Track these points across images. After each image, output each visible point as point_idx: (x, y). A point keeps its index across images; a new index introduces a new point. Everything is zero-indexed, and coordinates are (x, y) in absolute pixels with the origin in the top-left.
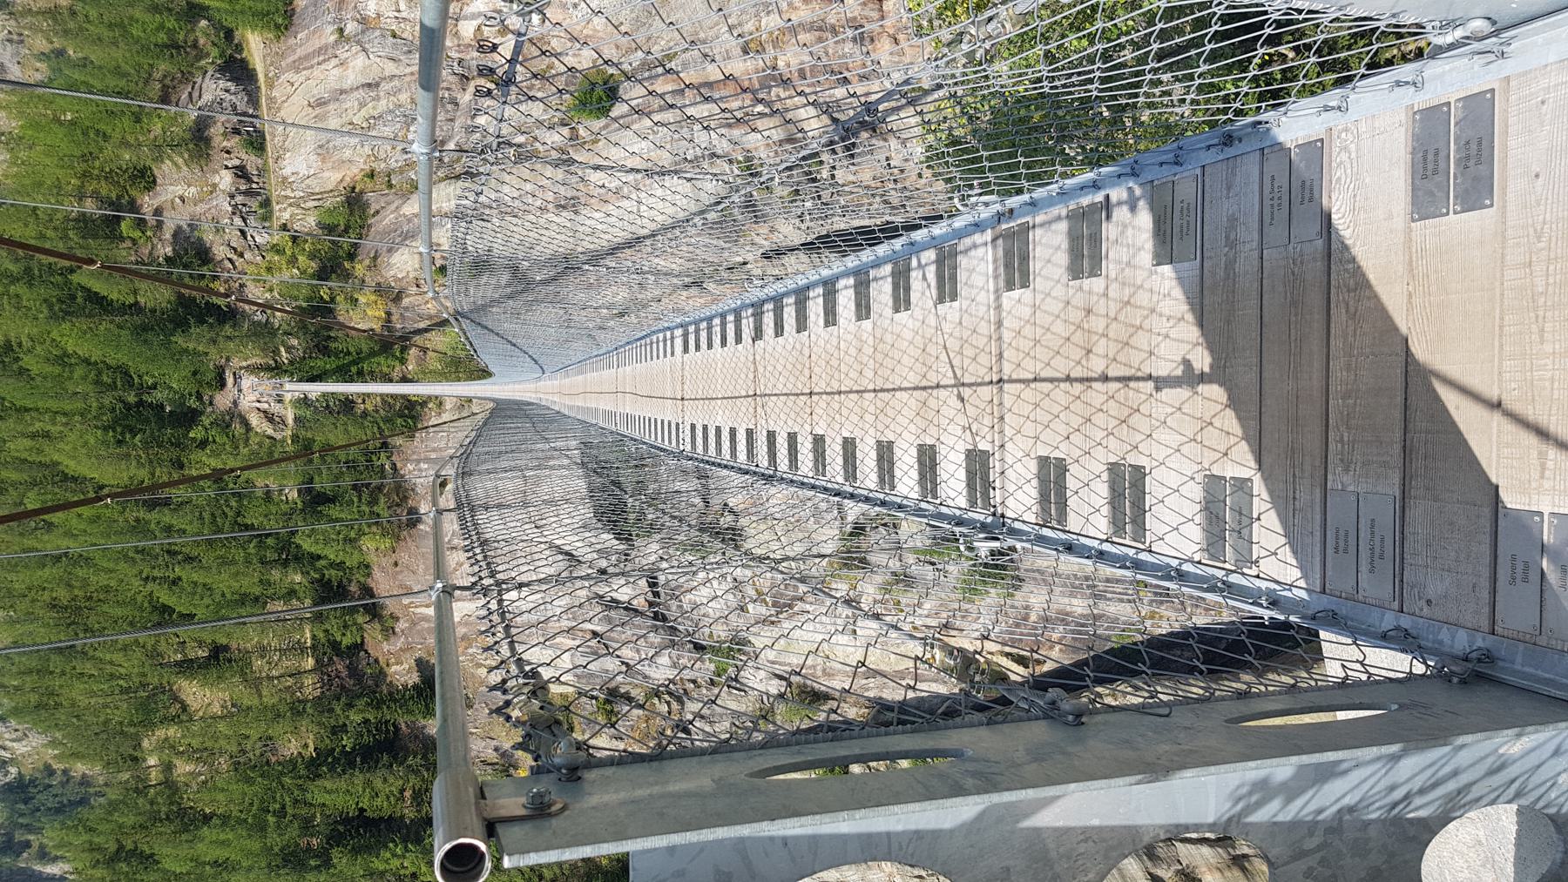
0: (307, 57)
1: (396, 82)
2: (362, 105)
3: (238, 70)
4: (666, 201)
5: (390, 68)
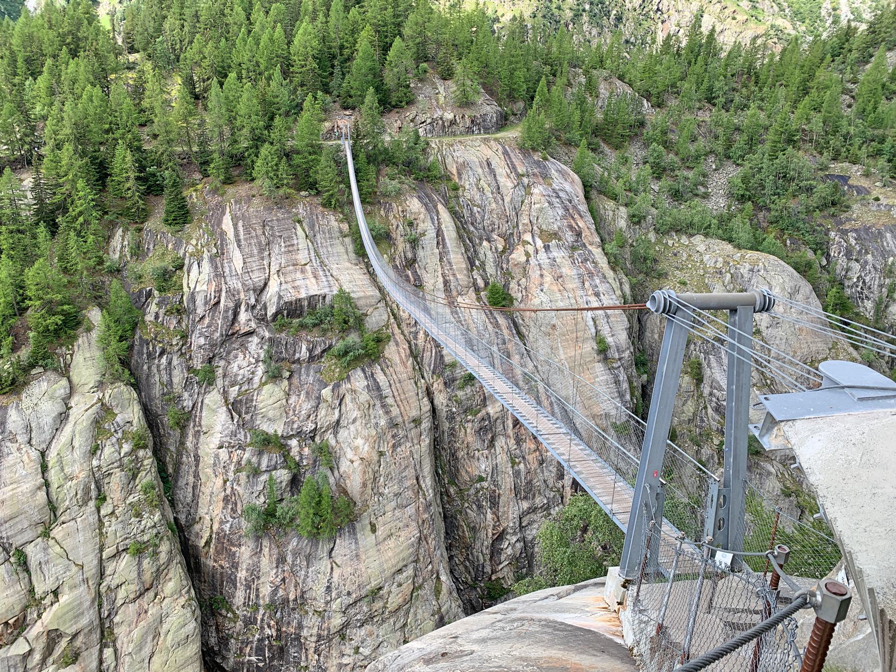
0: (510, 158)
1: (501, 202)
3: (503, 122)
5: (507, 199)
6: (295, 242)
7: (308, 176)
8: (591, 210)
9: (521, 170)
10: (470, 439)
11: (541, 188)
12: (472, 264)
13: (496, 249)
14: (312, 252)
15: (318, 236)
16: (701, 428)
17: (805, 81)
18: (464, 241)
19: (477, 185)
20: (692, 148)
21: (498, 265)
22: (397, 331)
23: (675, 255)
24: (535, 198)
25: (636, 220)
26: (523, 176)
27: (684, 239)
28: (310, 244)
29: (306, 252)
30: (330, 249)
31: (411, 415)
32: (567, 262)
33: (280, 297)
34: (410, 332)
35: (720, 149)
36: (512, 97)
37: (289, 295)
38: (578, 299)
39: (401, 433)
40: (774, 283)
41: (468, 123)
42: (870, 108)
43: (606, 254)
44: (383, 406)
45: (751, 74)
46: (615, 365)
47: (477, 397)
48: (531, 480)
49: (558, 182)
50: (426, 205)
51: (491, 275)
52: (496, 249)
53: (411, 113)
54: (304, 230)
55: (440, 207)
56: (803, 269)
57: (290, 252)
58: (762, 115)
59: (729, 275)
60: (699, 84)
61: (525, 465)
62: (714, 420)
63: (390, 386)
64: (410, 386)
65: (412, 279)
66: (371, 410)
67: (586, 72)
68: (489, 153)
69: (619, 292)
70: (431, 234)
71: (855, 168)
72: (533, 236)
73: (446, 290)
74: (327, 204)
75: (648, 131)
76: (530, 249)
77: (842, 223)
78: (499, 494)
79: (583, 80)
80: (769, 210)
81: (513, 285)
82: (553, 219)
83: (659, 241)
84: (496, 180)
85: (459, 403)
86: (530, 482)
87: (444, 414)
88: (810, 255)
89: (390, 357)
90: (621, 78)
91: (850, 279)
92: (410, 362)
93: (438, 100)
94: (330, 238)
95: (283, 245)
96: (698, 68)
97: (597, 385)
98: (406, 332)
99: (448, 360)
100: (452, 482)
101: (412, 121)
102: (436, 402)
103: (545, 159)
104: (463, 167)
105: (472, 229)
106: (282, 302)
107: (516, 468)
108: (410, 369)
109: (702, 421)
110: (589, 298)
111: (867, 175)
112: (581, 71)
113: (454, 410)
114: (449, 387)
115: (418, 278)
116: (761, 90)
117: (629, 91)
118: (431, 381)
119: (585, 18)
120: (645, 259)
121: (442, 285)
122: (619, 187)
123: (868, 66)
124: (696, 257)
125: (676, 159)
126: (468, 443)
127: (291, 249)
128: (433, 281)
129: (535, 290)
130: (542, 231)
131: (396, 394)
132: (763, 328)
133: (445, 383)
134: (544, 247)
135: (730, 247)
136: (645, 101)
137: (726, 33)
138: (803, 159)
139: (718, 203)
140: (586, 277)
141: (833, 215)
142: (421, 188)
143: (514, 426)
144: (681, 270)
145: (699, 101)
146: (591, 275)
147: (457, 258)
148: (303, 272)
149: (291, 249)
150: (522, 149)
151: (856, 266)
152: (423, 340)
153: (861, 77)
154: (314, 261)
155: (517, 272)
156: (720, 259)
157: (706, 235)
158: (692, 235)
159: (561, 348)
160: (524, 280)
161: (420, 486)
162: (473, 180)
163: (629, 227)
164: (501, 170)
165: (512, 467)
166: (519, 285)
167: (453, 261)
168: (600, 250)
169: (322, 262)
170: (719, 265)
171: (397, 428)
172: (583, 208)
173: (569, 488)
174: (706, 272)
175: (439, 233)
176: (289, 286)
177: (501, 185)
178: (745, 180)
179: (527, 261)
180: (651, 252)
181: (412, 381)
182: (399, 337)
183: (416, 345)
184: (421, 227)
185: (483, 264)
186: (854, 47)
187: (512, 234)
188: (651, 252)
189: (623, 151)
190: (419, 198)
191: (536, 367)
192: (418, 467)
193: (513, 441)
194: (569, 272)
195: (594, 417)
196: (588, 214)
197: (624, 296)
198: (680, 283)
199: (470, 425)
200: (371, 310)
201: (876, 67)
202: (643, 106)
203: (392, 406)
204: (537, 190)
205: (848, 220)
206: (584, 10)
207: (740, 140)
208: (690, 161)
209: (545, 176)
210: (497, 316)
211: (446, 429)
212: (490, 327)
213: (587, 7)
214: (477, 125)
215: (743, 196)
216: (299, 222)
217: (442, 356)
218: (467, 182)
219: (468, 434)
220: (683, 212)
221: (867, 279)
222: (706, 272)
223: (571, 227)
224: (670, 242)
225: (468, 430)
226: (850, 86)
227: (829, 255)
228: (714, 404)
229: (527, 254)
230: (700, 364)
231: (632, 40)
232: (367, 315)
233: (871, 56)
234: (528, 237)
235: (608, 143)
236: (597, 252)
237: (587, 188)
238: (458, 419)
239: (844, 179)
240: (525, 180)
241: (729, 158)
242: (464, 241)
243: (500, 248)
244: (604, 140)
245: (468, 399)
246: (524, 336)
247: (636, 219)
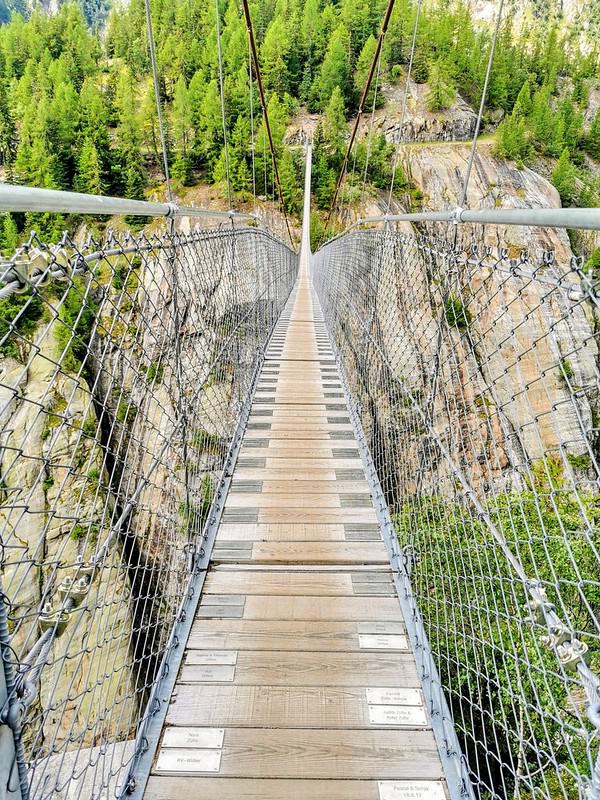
0: (481, 167)
3: (482, 128)
11: (512, 199)
93: (407, 103)
99: (394, 375)
101: (379, 126)
103: (520, 169)
104: (429, 175)
142: (382, 196)
150: (496, 157)
162: (439, 189)
177: (468, 195)
199: (413, 444)
209: (519, 187)
214: (449, 131)
223: (542, 243)
244: (589, 154)
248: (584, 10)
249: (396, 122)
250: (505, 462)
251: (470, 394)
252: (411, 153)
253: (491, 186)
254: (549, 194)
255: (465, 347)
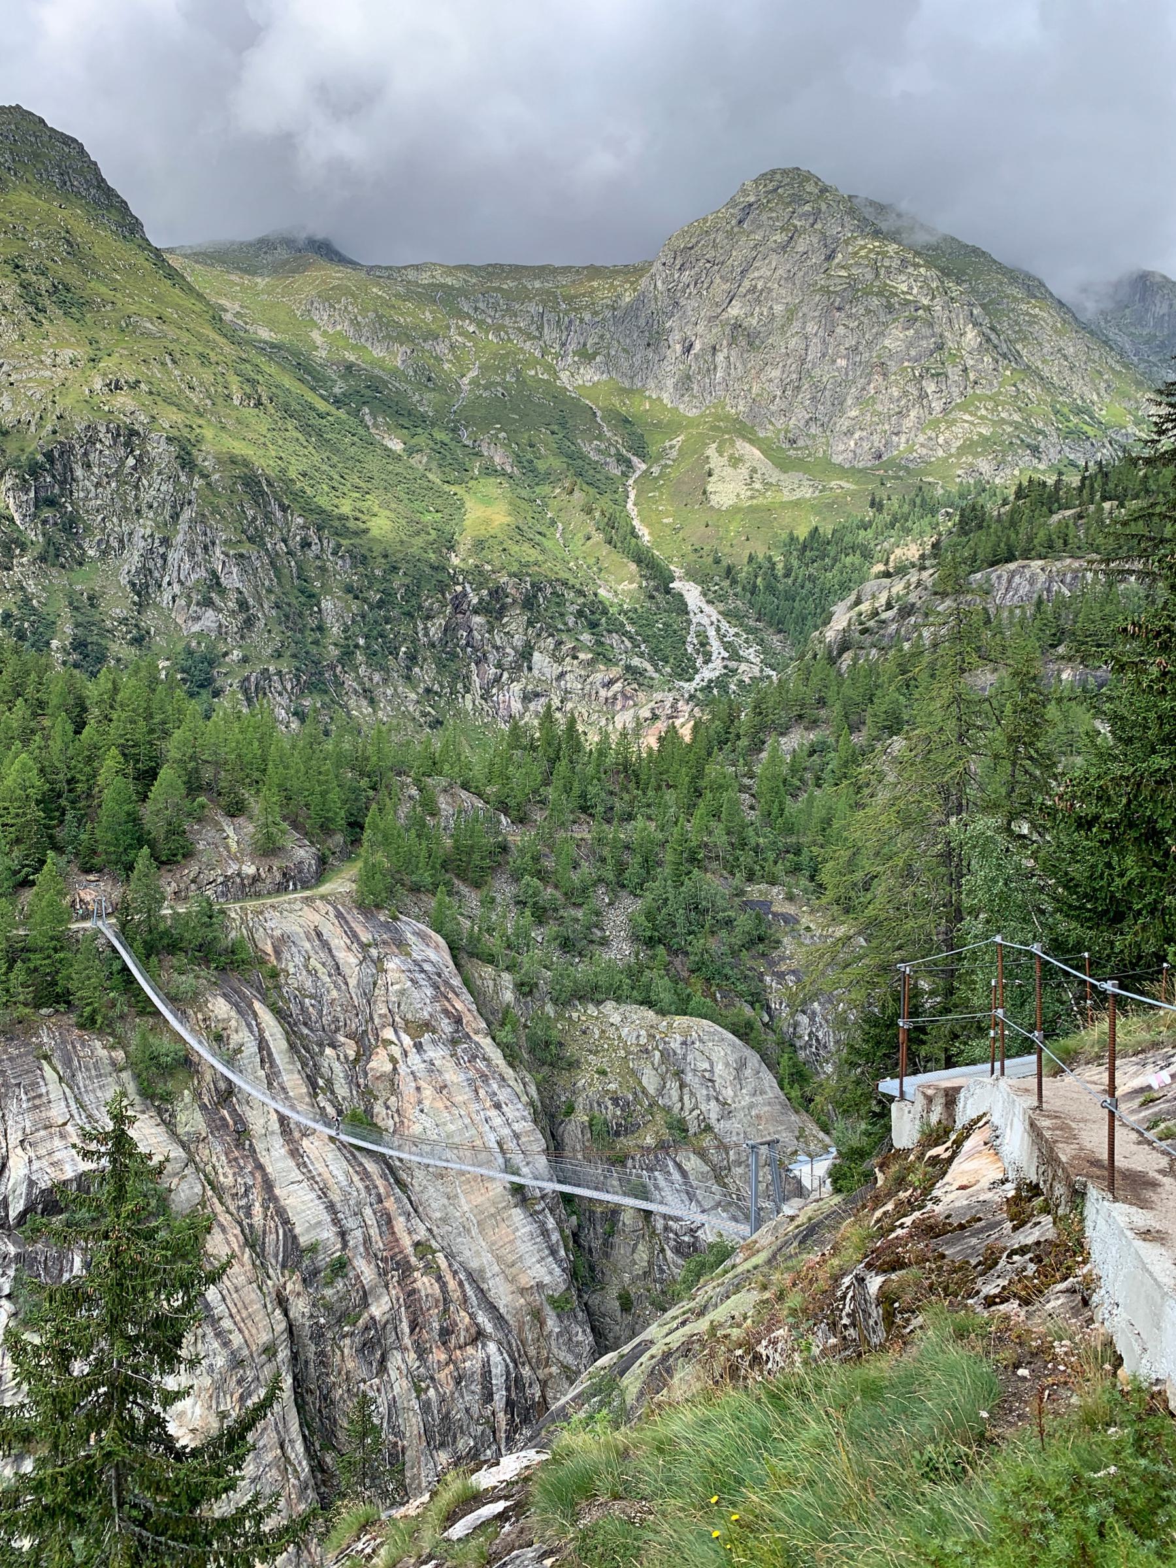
0: (347, 922)
1: (344, 987)
2: (324, 964)
3: (323, 868)
4: (304, 1208)
5: (353, 982)
6: (43, 1090)
7: (54, 983)
8: (466, 982)
9: (365, 937)
10: (350, 1365)
11: (397, 960)
12: (313, 1085)
13: (346, 1057)
14: (72, 1102)
15: (79, 1076)
16: (662, 1281)
17: (694, 778)
18: (297, 1052)
19: (306, 967)
20: (575, 877)
21: (352, 1081)
22: (219, 1208)
23: (584, 1033)
24: (391, 976)
25: (525, 988)
26: (369, 946)
27: (592, 1010)
28: (67, 1090)
29: (63, 1103)
30: (99, 1094)
31: (260, 1342)
32: (450, 1064)
33: (32, 1184)
34: (239, 1208)
35: (611, 877)
36: (326, 829)
37: (46, 1177)
38: (474, 1116)
39: (250, 1374)
40: (714, 1059)
41: (278, 877)
42: (775, 811)
43: (498, 1045)
44: (218, 1335)
45: (628, 771)
46: (538, 1208)
47: (354, 1294)
48: (448, 1413)
49: (419, 950)
50: (236, 1005)
51: (344, 1099)
52: (346, 1057)
53: (192, 870)
54: (55, 1069)
55: (257, 1005)
56: (743, 1031)
57: (36, 1107)
58: (652, 826)
59: (657, 1053)
60: (568, 790)
61: (436, 1389)
62: (677, 1267)
63: (224, 1299)
64: (251, 1294)
65: (231, 1122)
66: (199, 1345)
67: (417, 782)
68: (316, 918)
69: (525, 1099)
70: (251, 1048)
71: (775, 890)
72: (396, 1032)
73: (283, 1133)
74: (88, 1023)
75: (514, 860)
76: (396, 1051)
77: (775, 964)
78: (403, 1447)
79: (414, 791)
80: (686, 954)
81: (378, 1108)
82: (422, 1002)
83: (560, 1016)
84: (333, 956)
85: (329, 1308)
86: (446, 1417)
87: (307, 1332)
88: (748, 1011)
89: (215, 1252)
90: (465, 786)
91: (800, 1037)
92: (247, 1256)
93: (228, 847)
94: (97, 1077)
95: (24, 1097)
96: (562, 767)
97: (518, 1242)
98: (232, 1209)
99: (304, 1241)
100: (328, 1446)
101: (193, 881)
102: (291, 1315)
103: (396, 919)
104: (282, 943)
105: (306, 1031)
106: (36, 1191)
107: (424, 1397)
108: (249, 1267)
109: (662, 1271)
110: (489, 1113)
111: (790, 898)
112: (409, 780)
113: (322, 1321)
114: (311, 1286)
115: (239, 1119)
116: (644, 793)
117: (480, 804)
118: (282, 1280)
119: (360, 657)
120: (547, 1044)
121: (277, 1125)
122: (493, 943)
123: (764, 755)
124: (611, 1032)
125: (558, 894)
126: (348, 1372)
127: (37, 1102)
128: (262, 1121)
129: (411, 1112)
130: (407, 1022)
131: (234, 1311)
132: (713, 1122)
133: (304, 1280)
134: (415, 1045)
135: (651, 1013)
136: (502, 817)
137: (567, 677)
138: (713, 884)
139: (620, 951)
140: (479, 1083)
141: (763, 955)
142: (224, 981)
143: (412, 1331)
144: (596, 1053)
145: (572, 812)
146: (485, 1078)
147: (293, 1080)
148: (63, 1136)
149: (37, 1102)
150: (361, 907)
151: (804, 1020)
152: (261, 1216)
153: (758, 769)
154: (77, 1117)
155: (381, 1088)
156: (643, 1032)
157: (618, 1000)
158: (599, 1003)
159: (461, 1195)
160: (393, 1099)
161: (288, 1460)
162: (299, 960)
163: (517, 1000)
164: (338, 941)
165: (418, 1397)
166: (388, 1108)
167: (287, 1085)
168: (489, 1040)
169: (89, 1116)
170: (643, 1041)
171: (243, 1367)
172: (456, 982)
173: (502, 1414)
174: (628, 1053)
175: (263, 1045)
176: (44, 1163)
177: (341, 962)
178: (650, 916)
179: (395, 1069)
180: (554, 1033)
181: (254, 1285)
182: (224, 1219)
183: (251, 1226)
184: (235, 1039)
185: (329, 1082)
186: (742, 732)
187: (365, 1032)
188: (554, 1033)
189: (485, 889)
190: (225, 996)
191: (430, 1230)
192: (280, 1426)
193: (413, 1355)
194: (455, 1078)
195: (522, 1291)
196: (465, 990)
197: (532, 1103)
198: (598, 1072)
199: (347, 1341)
200: (175, 1181)
201: (773, 758)
202: (499, 822)
203: (230, 1332)
204: (392, 964)
205: (782, 958)
206: (357, 646)
207: (634, 862)
208: (576, 896)
209: (400, 944)
210: (364, 1160)
211: (312, 1356)
212: (356, 1178)
213: (361, 642)
214: (290, 880)
215: (651, 938)
216: (46, 1057)
217: (295, 1237)
218: (292, 963)
219: (347, 1357)
220: (582, 970)
221: (820, 1035)
222: (628, 1053)
223: (446, 1012)
224: (575, 1015)
225: (346, 1351)
226: (746, 781)
227: (769, 1007)
228: (672, 1243)
229: (393, 1060)
230: (644, 1187)
231: (436, 687)
232: (171, 1191)
233: (764, 743)
234: (388, 1033)
235: (464, 880)
236: (486, 1042)
237: (454, 949)
238: (330, 1335)
239: (767, 905)
240: (374, 952)
241: (623, 886)
242: (297, 1052)
243: (352, 1054)
244: (458, 876)
245: (341, 1299)
246: (405, 1186)
247: (526, 989)
248: (353, 621)
249: (216, 874)
250: (473, 1330)
251: (406, 1242)
252: (250, 916)
253: (364, 947)
254: (437, 947)
255: (384, 1176)
